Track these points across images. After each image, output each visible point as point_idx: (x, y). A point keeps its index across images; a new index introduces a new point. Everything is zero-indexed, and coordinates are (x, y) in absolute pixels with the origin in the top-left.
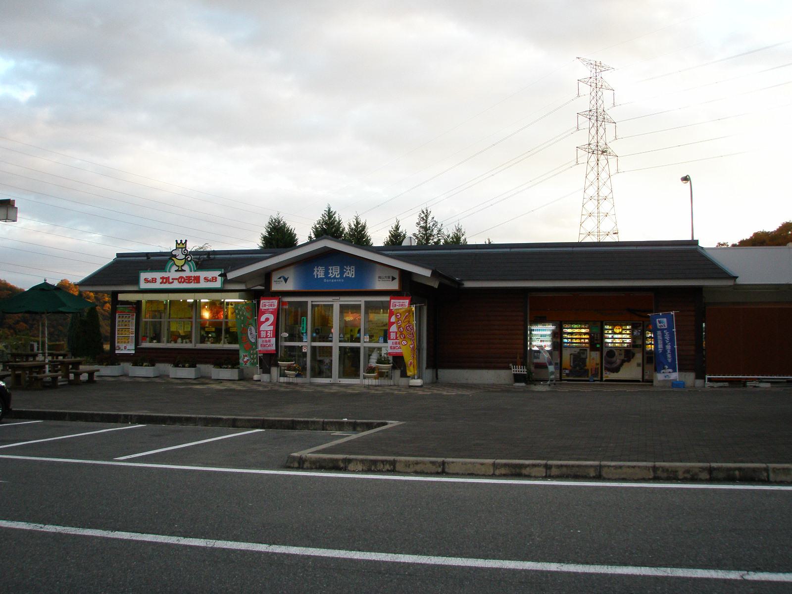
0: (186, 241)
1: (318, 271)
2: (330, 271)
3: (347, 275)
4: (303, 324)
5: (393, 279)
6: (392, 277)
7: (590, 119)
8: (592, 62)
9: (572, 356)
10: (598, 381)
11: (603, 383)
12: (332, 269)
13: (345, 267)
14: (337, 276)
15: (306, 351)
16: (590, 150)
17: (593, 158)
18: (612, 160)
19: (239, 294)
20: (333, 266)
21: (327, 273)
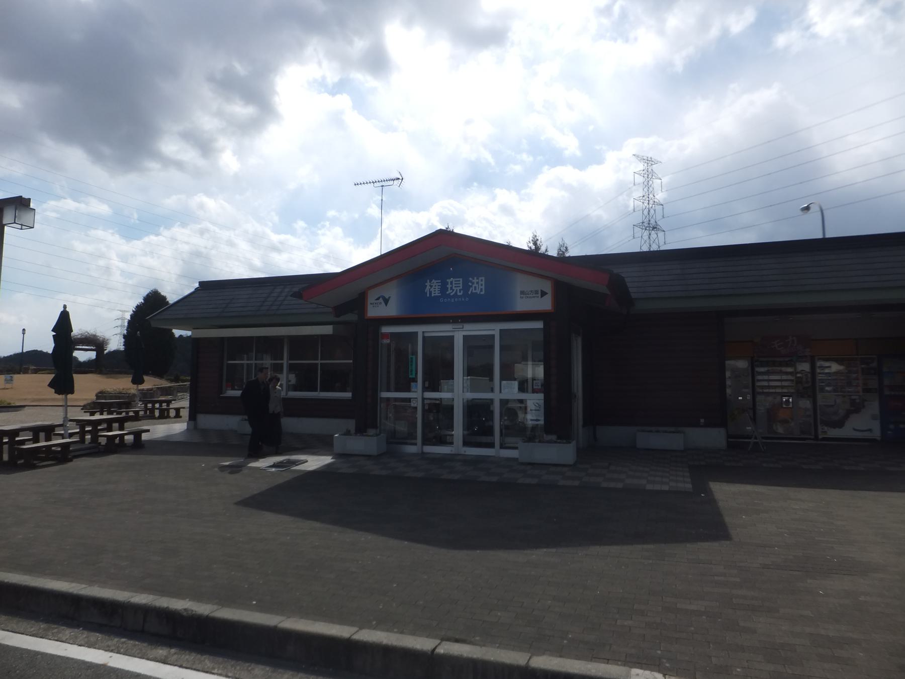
1: (431, 286)
2: (449, 286)
3: (474, 291)
4: (412, 365)
5: (543, 294)
6: (542, 291)
7: (643, 203)
8: (645, 158)
10: (810, 439)
11: (819, 442)
12: (451, 283)
13: (471, 279)
14: (459, 294)
15: (415, 405)
16: (644, 227)
17: (646, 233)
18: (661, 234)
19: (333, 327)
21: (443, 288)
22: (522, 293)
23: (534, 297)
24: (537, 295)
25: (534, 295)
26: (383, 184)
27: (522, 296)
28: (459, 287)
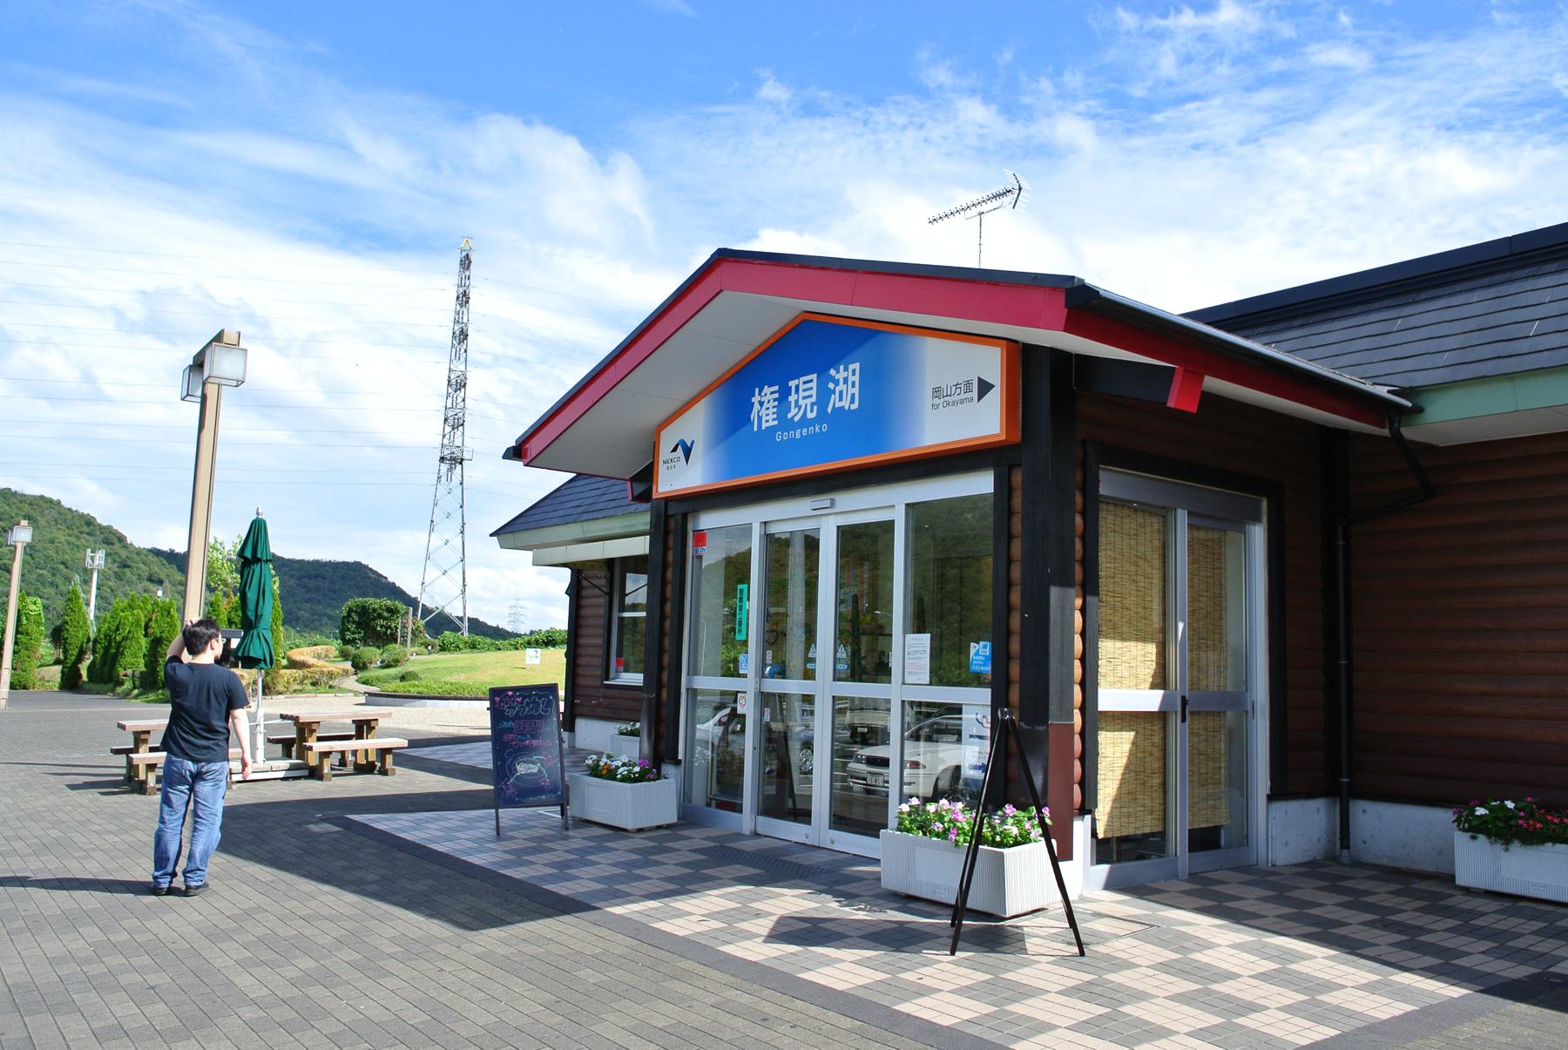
0: (693, 442)
3: (838, 405)
9: (788, 536)
13: (832, 372)
20: (798, 378)
22: (937, 392)
23: (962, 402)
24: (969, 395)
25: (963, 396)
26: (980, 209)
27: (937, 401)
28: (811, 396)
